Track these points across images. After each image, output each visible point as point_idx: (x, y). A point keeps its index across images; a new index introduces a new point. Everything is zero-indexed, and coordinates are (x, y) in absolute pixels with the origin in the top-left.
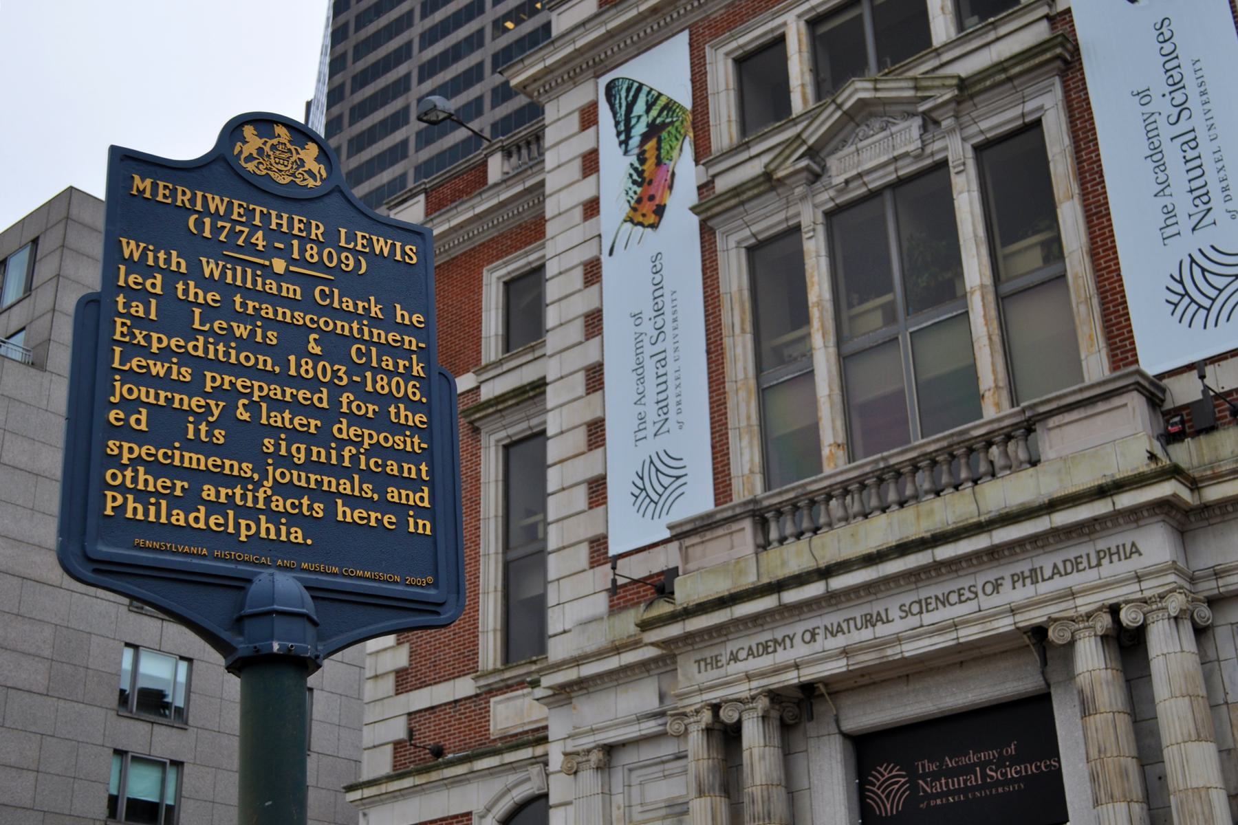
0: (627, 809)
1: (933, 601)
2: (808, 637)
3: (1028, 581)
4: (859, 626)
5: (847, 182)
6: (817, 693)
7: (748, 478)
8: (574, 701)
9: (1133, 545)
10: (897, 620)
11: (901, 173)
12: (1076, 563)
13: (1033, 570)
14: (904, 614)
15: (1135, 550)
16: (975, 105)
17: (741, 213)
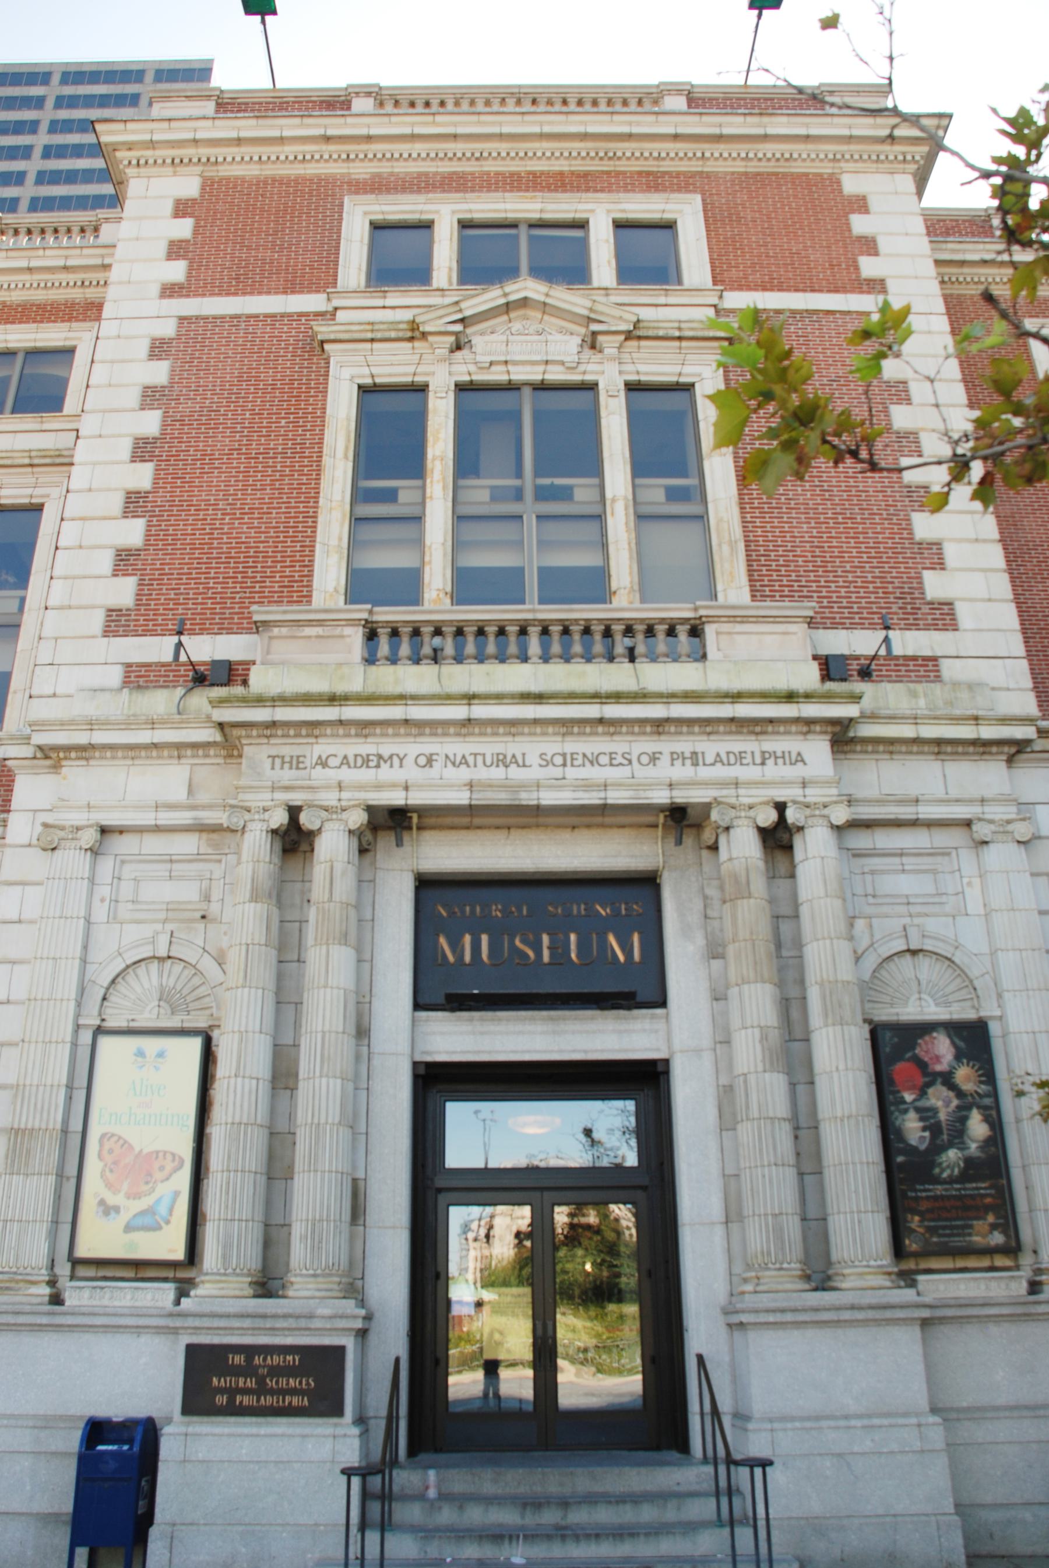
0: (113, 903)
1: (580, 757)
2: (422, 761)
3: (688, 762)
4: (488, 763)
5: (491, 363)
6: (406, 824)
7: (331, 595)
8: (64, 770)
9: (799, 754)
10: (536, 767)
11: (548, 377)
12: (740, 757)
13: (694, 754)
14: (544, 763)
15: (800, 759)
16: (639, 347)
17: (365, 350)
